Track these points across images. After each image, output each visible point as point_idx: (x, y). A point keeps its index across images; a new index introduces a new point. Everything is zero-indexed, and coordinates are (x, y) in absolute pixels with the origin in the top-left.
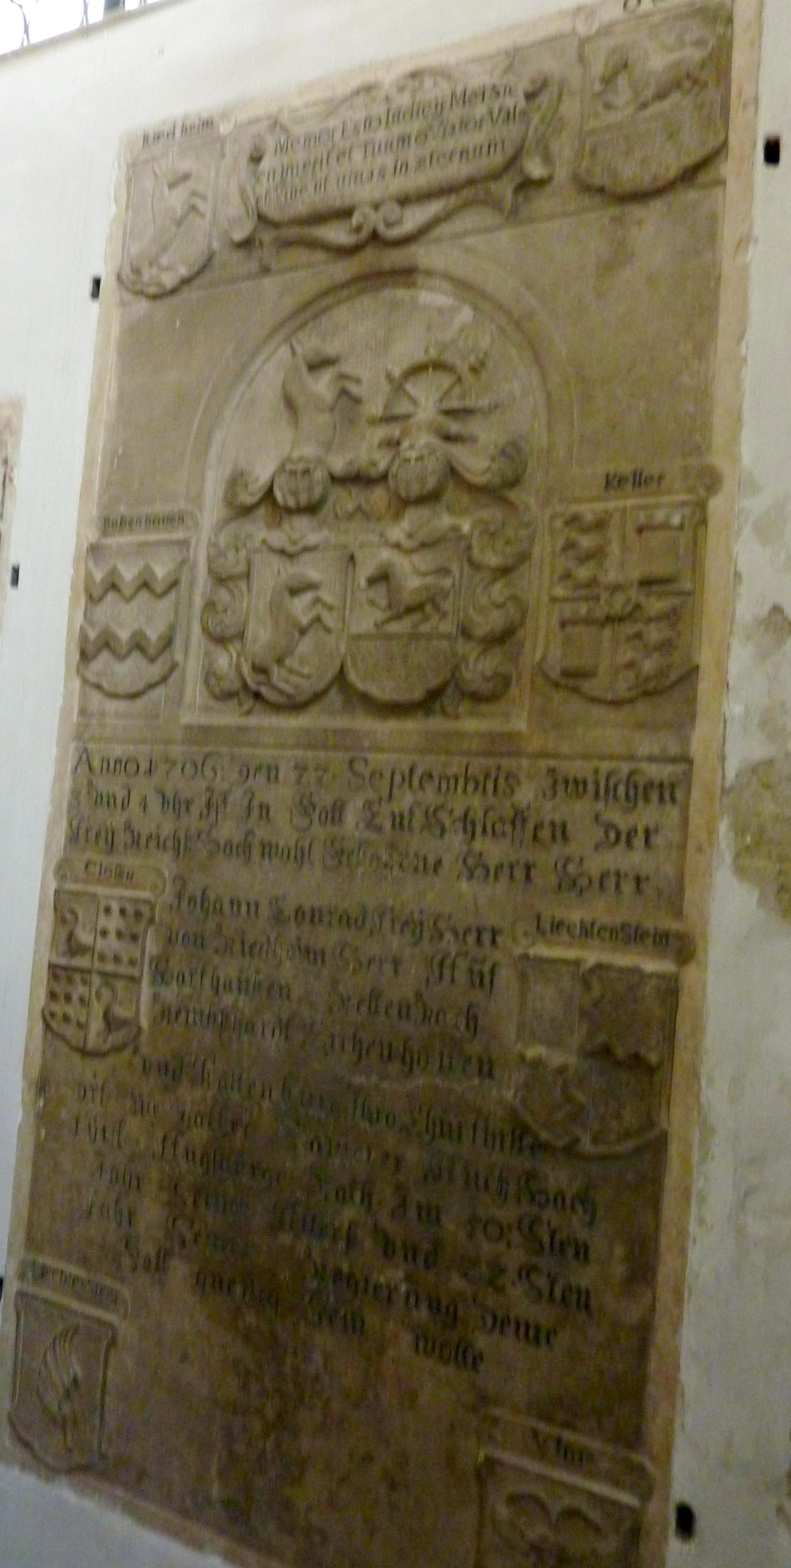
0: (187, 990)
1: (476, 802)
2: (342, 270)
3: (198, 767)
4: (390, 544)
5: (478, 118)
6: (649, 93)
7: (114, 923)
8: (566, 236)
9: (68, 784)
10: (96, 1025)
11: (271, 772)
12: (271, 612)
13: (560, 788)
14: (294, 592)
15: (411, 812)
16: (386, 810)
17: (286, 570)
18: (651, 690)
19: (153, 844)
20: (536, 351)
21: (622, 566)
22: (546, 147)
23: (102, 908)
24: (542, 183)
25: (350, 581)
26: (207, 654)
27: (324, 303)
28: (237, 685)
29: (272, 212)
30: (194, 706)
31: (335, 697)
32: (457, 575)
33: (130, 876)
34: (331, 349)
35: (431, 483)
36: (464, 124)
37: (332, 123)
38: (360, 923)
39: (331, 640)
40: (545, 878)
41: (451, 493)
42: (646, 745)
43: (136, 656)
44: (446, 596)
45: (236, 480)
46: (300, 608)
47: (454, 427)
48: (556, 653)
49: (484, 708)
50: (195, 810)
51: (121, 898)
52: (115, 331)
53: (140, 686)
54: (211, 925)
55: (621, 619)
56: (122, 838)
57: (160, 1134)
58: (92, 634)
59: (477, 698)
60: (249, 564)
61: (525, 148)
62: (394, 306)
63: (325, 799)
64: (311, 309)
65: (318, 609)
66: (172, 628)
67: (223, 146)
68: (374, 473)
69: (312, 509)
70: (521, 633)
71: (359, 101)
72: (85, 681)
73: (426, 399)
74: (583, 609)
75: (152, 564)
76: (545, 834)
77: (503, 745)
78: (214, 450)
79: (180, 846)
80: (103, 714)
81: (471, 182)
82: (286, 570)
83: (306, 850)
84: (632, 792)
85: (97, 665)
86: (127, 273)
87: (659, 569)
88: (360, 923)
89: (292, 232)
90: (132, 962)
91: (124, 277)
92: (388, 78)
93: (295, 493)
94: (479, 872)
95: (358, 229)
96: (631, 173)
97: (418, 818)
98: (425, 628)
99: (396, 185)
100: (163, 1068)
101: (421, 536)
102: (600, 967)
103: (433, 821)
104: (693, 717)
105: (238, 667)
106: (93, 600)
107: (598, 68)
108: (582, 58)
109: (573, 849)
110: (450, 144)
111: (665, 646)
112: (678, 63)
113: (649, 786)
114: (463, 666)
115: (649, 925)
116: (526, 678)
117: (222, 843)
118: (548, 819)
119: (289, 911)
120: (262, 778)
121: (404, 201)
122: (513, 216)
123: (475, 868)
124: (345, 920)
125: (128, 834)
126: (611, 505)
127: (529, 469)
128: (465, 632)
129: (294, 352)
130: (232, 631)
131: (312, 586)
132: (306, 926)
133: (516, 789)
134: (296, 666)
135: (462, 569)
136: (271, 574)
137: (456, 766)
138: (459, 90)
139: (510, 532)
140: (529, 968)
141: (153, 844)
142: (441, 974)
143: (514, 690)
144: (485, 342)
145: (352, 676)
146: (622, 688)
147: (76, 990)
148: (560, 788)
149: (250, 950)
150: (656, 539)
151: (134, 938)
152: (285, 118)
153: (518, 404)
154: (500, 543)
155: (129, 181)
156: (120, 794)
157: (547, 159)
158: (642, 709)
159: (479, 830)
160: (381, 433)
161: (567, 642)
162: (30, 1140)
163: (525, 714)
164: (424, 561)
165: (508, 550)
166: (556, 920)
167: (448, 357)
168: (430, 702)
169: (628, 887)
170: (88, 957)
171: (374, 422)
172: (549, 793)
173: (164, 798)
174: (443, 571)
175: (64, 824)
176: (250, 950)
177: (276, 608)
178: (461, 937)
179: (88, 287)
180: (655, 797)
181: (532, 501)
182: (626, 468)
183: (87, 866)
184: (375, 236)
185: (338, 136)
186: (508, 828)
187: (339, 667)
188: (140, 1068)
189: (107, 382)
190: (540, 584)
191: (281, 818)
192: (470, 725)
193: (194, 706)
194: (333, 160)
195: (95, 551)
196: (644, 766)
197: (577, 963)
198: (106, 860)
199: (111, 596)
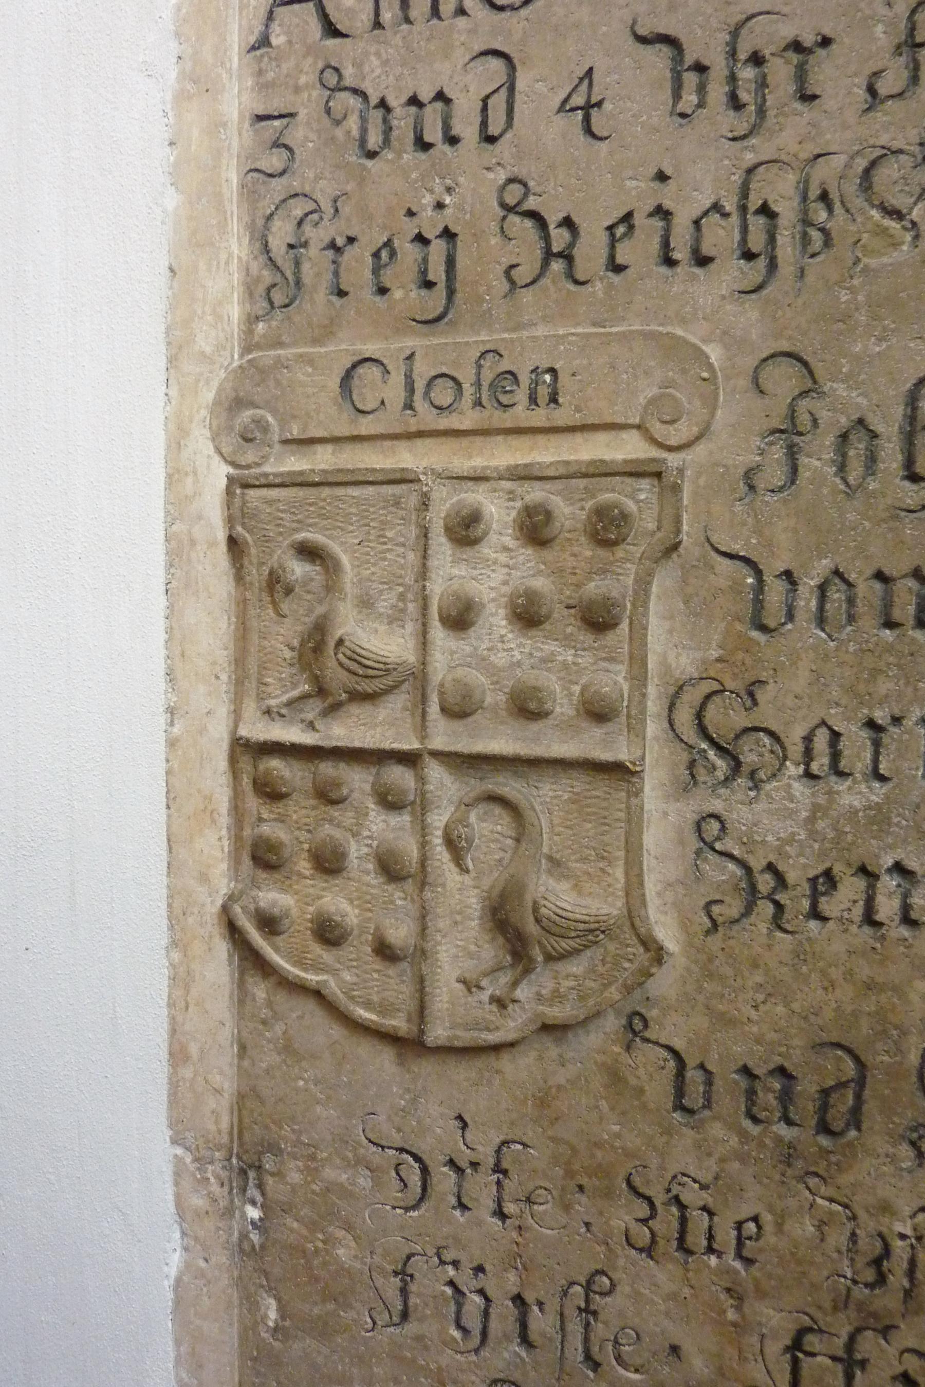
7: (495, 572)
9: (235, 100)
10: (460, 949)
19: (639, 251)
33: (548, 388)
50: (837, 78)
51: (524, 475)
56: (491, 251)
57: (776, 1319)
90: (597, 712)
100: (769, 1088)
141: (639, 251)
151: (598, 620)
156: (470, 86)
162: (223, 1334)
170: (397, 704)
175: (237, 246)
188: (658, 1089)
198: (431, 351)
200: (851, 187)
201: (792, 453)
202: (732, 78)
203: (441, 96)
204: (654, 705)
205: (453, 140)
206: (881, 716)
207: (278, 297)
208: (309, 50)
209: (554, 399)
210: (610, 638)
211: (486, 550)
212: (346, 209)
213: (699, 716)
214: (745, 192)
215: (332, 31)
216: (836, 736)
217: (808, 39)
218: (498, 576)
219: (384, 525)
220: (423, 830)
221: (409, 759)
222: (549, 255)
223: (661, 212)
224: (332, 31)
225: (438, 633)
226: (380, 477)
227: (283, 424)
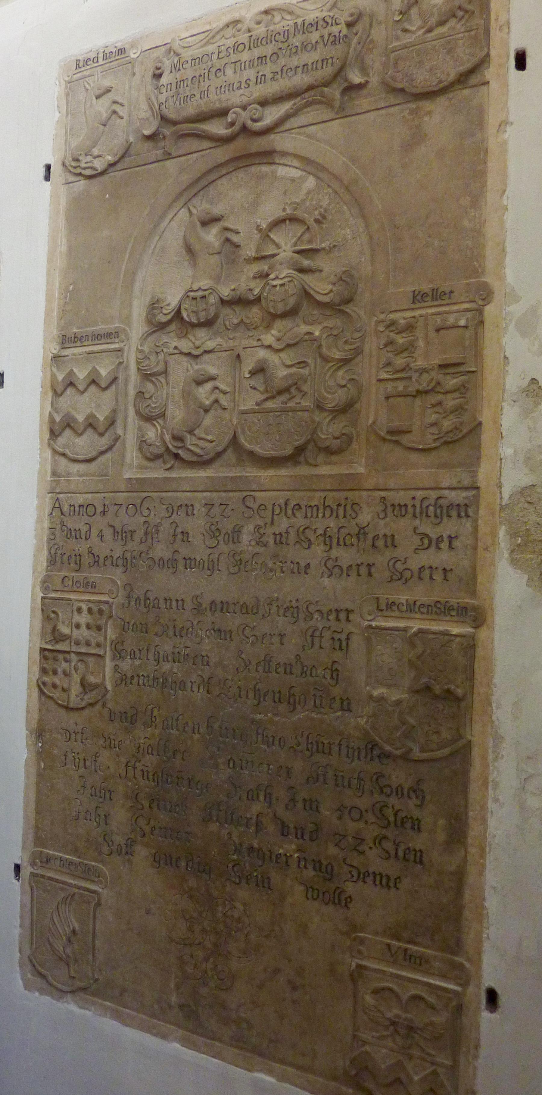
21: (426, 356)
55: (426, 392)
74: (400, 387)
87: (452, 356)
104: (479, 458)
111: (458, 410)
150: (451, 335)
158: (444, 454)
182: (426, 287)
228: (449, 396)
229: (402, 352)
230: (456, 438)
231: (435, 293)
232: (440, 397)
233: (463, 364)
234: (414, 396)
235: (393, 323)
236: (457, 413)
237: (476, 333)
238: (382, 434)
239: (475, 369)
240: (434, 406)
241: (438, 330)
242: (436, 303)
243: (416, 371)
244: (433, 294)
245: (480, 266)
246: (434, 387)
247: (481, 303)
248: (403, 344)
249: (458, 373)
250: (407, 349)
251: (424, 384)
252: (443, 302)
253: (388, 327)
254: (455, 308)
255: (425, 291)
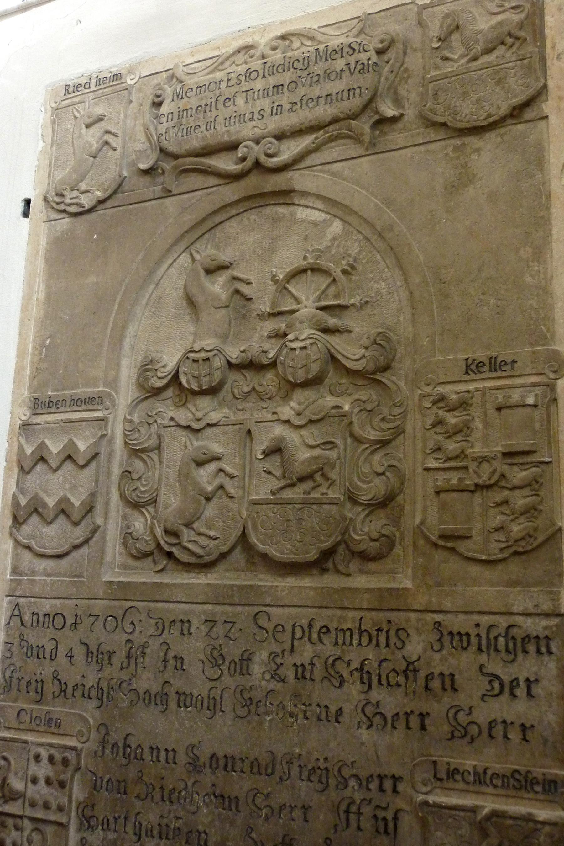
0: (111, 836)
1: (370, 654)
2: (231, 192)
3: (119, 621)
4: (280, 421)
5: (338, 70)
6: (479, 48)
7: (43, 770)
8: (418, 162)
11: (184, 625)
12: (180, 481)
13: (446, 639)
14: (200, 464)
15: (312, 664)
16: (289, 660)
17: (192, 444)
18: (520, 551)
19: (78, 693)
20: (396, 255)
22: (396, 93)
23: (31, 757)
24: (394, 120)
25: (248, 452)
26: (125, 517)
27: (218, 219)
28: (152, 546)
29: (173, 148)
30: (113, 566)
31: (238, 555)
32: (342, 447)
34: (224, 257)
35: (315, 368)
36: (327, 75)
37: (218, 75)
38: (269, 771)
39: (233, 505)
40: (439, 727)
41: (332, 377)
42: (520, 601)
43: (62, 519)
44: (333, 467)
45: (147, 367)
46: (205, 476)
47: (332, 321)
48: (433, 517)
49: (372, 566)
50: (116, 661)
51: (51, 745)
52: (43, 242)
53: (66, 548)
54: (132, 773)
55: (488, 487)
56: (51, 688)
58: (23, 502)
59: (364, 557)
60: (159, 437)
61: (379, 93)
62: (276, 220)
63: (234, 651)
64: (206, 225)
65: (221, 479)
66: (93, 495)
67: (130, 93)
68: (265, 361)
69: (212, 391)
70: (400, 499)
71: (241, 58)
72: (17, 542)
73: (307, 297)
74: (455, 478)
75: (75, 440)
76: (436, 684)
77: (390, 600)
78: (127, 342)
79: (102, 695)
80: (33, 573)
81: (335, 120)
82: (192, 444)
83: (218, 698)
84: (511, 645)
85: (26, 529)
86: (53, 197)
87: (520, 442)
88: (269, 771)
89: (189, 162)
90: (60, 809)
91: (50, 198)
92: (263, 41)
93: (197, 378)
94: (377, 720)
95: (243, 159)
96: (467, 112)
97: (319, 672)
98: (316, 495)
99: (273, 124)
101: (309, 415)
102: (495, 814)
103: (334, 676)
105: (153, 533)
106: (24, 471)
107: (435, 30)
108: (420, 23)
109: (462, 699)
110: (317, 91)
111: (531, 511)
112: (500, 24)
113: (527, 638)
114: (351, 528)
115: (537, 772)
116: (408, 540)
117: (141, 692)
118: (437, 671)
119: (204, 759)
120: (176, 631)
121: (280, 137)
122: (373, 148)
123: (374, 717)
124: (256, 767)
125: (56, 682)
126: (471, 387)
127: (398, 355)
128: (352, 499)
129: (193, 260)
130: (146, 497)
131: (217, 458)
132: (220, 773)
133: (407, 642)
134: (204, 530)
135: (345, 444)
136: (178, 447)
137: (351, 619)
138: (322, 47)
139: (385, 411)
140: (429, 813)
141: (78, 693)
142: (348, 820)
143: (398, 550)
144: (354, 250)
145: (253, 539)
146: (494, 550)
147: (9, 836)
148: (446, 639)
149: (170, 796)
151: (62, 785)
152: (179, 73)
153: (385, 301)
154: (376, 420)
155: (53, 122)
156: (49, 646)
157: (397, 101)
158: (514, 568)
159: (375, 679)
160: (270, 326)
161: (443, 506)
163: (410, 571)
164: (312, 435)
165: (384, 426)
166: (452, 768)
167: (323, 263)
168: (323, 562)
169: (514, 735)
171: (263, 317)
172: (437, 647)
173: (88, 649)
174: (329, 444)
176: (170, 796)
177: (184, 477)
178: (364, 783)
179: (20, 207)
180: (532, 648)
181: (402, 384)
182: (482, 355)
183: (19, 714)
184: (257, 164)
185: (223, 85)
186: (401, 679)
187: (242, 529)
189: (37, 285)
190: (413, 454)
191: (194, 668)
192: (360, 581)
193: (113, 566)
194: (220, 106)
195: (26, 427)
196: (520, 620)
197: (474, 810)
199: (40, 467)
200: (117, 687)
201: (104, 748)
202: (97, 657)
203: (43, 647)
204: (74, 808)
205: (45, 658)
206: (117, 815)
207: (6, 690)
208: (18, 629)
209: (59, 726)
210: (64, 790)
211: (42, 764)
212: (22, 670)
213: (83, 811)
214: (98, 684)
215: (22, 624)
216: (108, 820)
217: (111, 651)
218: (44, 771)
219: (21, 754)
220: (22, 837)
221: (21, 817)
222: (61, 692)
223: (83, 685)
224: (22, 624)
225: (30, 784)
226: (284, 502)
227: (4, 722)
228: (517, 492)
229: (455, 434)
230: (530, 548)
231: (493, 362)
232: (506, 493)
233: (535, 452)
234: (472, 492)
235: (442, 398)
236: (528, 515)
237: (548, 416)
238: (433, 538)
239: (549, 460)
240: (498, 505)
241: (499, 409)
242: (494, 374)
243: (474, 460)
244: (490, 363)
245: (548, 331)
246: (498, 481)
247: (552, 376)
248: (455, 425)
249: (527, 463)
250: (461, 431)
251: (485, 477)
252: (504, 374)
253: (435, 403)
254: (519, 381)
255: (481, 360)
